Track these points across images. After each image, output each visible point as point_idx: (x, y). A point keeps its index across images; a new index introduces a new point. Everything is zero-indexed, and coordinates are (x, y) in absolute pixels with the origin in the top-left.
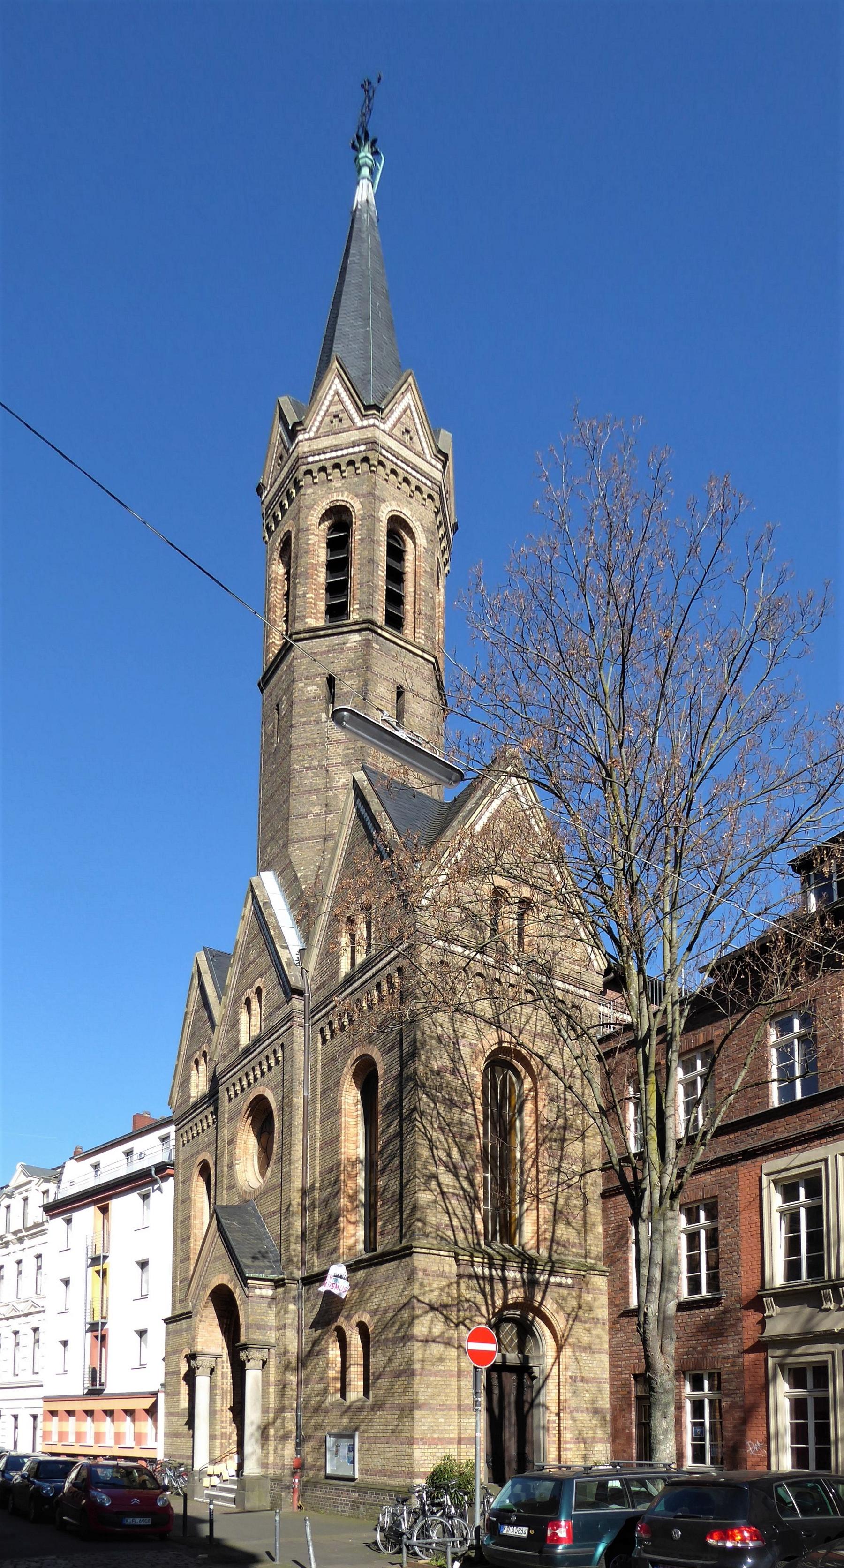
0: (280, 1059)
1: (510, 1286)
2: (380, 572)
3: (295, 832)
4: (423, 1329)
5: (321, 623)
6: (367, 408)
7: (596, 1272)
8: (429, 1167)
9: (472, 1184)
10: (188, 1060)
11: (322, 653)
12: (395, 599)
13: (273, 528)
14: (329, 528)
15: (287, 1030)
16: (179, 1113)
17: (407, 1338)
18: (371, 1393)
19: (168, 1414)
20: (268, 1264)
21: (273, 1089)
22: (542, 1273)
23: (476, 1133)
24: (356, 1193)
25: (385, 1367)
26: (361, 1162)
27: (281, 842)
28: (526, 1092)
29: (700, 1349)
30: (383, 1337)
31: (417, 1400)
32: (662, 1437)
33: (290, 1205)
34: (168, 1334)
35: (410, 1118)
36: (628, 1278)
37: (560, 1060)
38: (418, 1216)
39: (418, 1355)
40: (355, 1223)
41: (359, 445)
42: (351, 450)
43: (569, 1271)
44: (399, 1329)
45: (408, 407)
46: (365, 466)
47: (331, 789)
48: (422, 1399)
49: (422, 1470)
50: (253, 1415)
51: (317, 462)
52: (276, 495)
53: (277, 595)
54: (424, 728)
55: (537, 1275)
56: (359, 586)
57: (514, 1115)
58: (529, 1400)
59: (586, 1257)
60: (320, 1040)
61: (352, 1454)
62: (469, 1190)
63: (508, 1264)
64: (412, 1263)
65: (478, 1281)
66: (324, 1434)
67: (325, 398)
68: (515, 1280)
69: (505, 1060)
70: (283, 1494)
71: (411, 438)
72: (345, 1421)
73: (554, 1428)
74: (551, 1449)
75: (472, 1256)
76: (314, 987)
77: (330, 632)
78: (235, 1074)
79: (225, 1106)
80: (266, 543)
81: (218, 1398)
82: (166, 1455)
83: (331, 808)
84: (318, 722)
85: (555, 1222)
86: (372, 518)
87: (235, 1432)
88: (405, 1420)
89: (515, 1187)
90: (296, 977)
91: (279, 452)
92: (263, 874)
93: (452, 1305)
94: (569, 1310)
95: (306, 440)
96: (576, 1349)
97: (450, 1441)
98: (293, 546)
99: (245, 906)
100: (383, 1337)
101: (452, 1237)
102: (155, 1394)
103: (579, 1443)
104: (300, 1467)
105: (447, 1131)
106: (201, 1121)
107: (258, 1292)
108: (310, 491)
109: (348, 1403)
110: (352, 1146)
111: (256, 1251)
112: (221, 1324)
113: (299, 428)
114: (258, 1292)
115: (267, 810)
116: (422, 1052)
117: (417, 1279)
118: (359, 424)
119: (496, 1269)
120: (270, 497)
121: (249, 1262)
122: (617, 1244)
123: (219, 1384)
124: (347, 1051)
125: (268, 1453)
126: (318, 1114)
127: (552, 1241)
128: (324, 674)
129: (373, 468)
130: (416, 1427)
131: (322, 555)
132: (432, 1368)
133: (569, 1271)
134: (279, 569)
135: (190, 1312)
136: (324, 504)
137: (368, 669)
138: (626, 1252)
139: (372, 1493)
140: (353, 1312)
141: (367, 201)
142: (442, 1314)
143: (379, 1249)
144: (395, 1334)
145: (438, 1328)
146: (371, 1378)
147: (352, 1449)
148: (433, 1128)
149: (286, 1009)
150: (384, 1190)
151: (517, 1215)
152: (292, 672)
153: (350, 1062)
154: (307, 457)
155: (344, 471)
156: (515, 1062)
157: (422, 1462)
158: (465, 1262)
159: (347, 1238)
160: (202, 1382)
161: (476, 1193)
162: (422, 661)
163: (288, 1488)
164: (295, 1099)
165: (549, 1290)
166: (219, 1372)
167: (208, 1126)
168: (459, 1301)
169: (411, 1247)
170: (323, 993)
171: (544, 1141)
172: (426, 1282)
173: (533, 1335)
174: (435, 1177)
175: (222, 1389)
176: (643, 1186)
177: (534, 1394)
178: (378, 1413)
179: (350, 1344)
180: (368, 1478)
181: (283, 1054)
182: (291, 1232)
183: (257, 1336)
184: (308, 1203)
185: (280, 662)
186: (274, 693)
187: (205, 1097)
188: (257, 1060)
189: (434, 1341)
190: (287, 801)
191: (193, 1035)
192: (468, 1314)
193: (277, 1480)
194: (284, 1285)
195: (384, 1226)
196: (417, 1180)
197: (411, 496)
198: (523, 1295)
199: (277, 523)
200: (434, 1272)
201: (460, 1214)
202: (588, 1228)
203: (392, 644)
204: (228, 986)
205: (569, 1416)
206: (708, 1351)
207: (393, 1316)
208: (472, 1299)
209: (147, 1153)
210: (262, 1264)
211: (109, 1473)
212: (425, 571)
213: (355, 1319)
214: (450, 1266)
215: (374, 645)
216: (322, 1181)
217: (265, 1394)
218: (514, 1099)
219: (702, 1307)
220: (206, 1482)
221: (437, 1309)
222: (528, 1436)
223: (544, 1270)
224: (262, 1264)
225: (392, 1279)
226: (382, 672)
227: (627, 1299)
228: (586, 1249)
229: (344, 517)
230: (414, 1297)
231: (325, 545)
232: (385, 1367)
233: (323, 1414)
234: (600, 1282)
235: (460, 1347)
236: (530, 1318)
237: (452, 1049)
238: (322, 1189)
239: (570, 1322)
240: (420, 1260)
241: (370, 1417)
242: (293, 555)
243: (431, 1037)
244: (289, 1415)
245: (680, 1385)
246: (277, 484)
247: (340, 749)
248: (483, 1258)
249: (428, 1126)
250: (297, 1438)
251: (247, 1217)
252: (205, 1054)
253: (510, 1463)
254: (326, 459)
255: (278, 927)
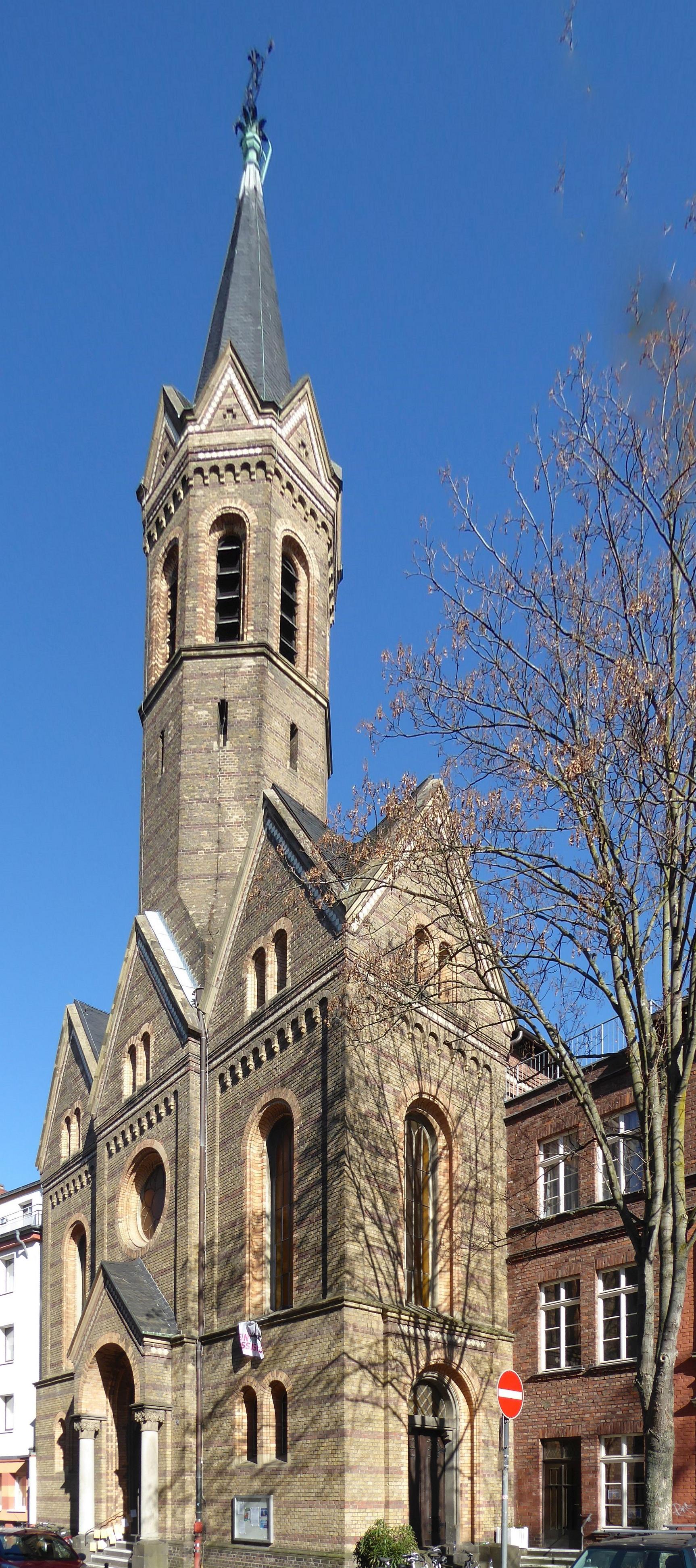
0: (172, 1108)
1: (432, 1346)
2: (275, 595)
3: (185, 866)
4: (353, 1388)
5: (212, 642)
6: (265, 404)
7: (504, 1338)
8: (357, 1217)
9: (396, 1240)
10: (57, 1119)
11: (213, 676)
12: (288, 631)
13: (156, 537)
14: (220, 541)
15: (181, 1076)
16: (48, 1174)
17: (340, 1397)
18: (289, 1455)
19: (41, 1478)
20: (163, 1322)
21: (163, 1141)
22: (460, 1336)
23: (399, 1186)
24: (262, 1248)
25: (307, 1428)
26: (267, 1216)
27: (168, 880)
28: (440, 1150)
29: (619, 1413)
30: (304, 1397)
31: (348, 1462)
32: (661, 1499)
33: (187, 1260)
34: (39, 1398)
35: (337, 1162)
36: (536, 1343)
37: (472, 1119)
38: (346, 1268)
39: (348, 1416)
40: (261, 1280)
41: (254, 447)
42: (245, 452)
43: (483, 1335)
44: (325, 1388)
45: (304, 418)
46: (260, 473)
47: (223, 825)
48: (352, 1461)
49: (353, 1535)
50: (149, 1479)
51: (208, 460)
52: (160, 498)
53: (160, 612)
54: (316, 775)
55: (456, 1337)
56: (253, 606)
57: (427, 1173)
58: (442, 1464)
59: (493, 1322)
60: (218, 1087)
61: (265, 1518)
62: (392, 1245)
63: (432, 1323)
64: (342, 1318)
65: (404, 1339)
66: (230, 1498)
67: (218, 387)
68: (437, 1342)
69: (421, 1114)
70: (185, 1559)
71: (307, 454)
72: (257, 1484)
73: (467, 1492)
74: (464, 1513)
75: (400, 1313)
76: (212, 1030)
77: (222, 652)
78: (117, 1127)
79: (105, 1163)
80: (147, 554)
81: (103, 1461)
82: (38, 1519)
83: (223, 846)
84: (209, 750)
85: (467, 1285)
86: (267, 531)
87: (122, 1496)
88: (333, 1483)
89: (428, 1248)
90: (193, 1018)
91: (164, 449)
92: (149, 914)
93: (379, 1364)
94: (482, 1374)
95: (197, 433)
96: (488, 1414)
97: (377, 1505)
98: (180, 554)
99: (129, 947)
100: (304, 1397)
101: (377, 1294)
102: (26, 1459)
103: (490, 1506)
104: (201, 1531)
105: (372, 1180)
106: (74, 1181)
107: (154, 1350)
108: (200, 492)
109: (259, 1465)
110: (257, 1199)
111: (150, 1309)
112: (105, 1386)
113: (189, 418)
114: (154, 1350)
115: (151, 847)
116: (351, 1092)
117: (347, 1335)
118: (255, 422)
119: (420, 1328)
120: (152, 501)
121: (144, 1319)
122: (524, 1310)
123: (104, 1447)
124: (252, 1097)
125: (166, 1517)
126: (217, 1166)
127: (465, 1304)
128: (216, 698)
129: (269, 476)
130: (347, 1491)
131: (211, 569)
132: (361, 1429)
133: (483, 1335)
134: (162, 585)
135: (72, 1374)
136: (216, 509)
137: (263, 698)
138: (535, 1318)
139: (293, 1559)
140: (266, 1371)
141: (255, 188)
142: (370, 1372)
143: (296, 1305)
144: (320, 1393)
145: (367, 1388)
146: (289, 1439)
147: (266, 1513)
148: (361, 1175)
149: (181, 1053)
150: (301, 1243)
151: (430, 1277)
152: (181, 693)
153: (256, 1109)
154: (197, 453)
155: (238, 475)
156: (430, 1117)
157: (352, 1527)
158: (392, 1319)
159: (254, 1295)
160: (86, 1446)
161: (399, 1248)
162: (315, 703)
163: (193, 1552)
164: (191, 1150)
165: (465, 1352)
166: (103, 1435)
167: (82, 1186)
168: (387, 1359)
169: (342, 1300)
170: (225, 1035)
171: (458, 1202)
172: (355, 1338)
173: (447, 1398)
174: (361, 1227)
175: (107, 1452)
176: (652, 1223)
177: (446, 1458)
178: (299, 1476)
179: (262, 1404)
180: (286, 1543)
181: (177, 1103)
182: (189, 1289)
183: (152, 1397)
184: (205, 1259)
185: (166, 684)
186: (159, 719)
187: (79, 1155)
188: (144, 1111)
189: (363, 1401)
190: (176, 834)
191: (63, 1092)
192: (395, 1374)
193: (177, 1545)
194: (182, 1344)
195: (302, 1280)
196: (346, 1229)
197: (305, 520)
198: (443, 1357)
199: (160, 530)
200: (364, 1328)
201: (384, 1269)
202: (495, 1294)
203: (286, 677)
204: (109, 1035)
205: (482, 1479)
206: (629, 1415)
207: (317, 1375)
208: (399, 1359)
209: (9, 1218)
210: (156, 1322)
211: (14, 1540)
212: (318, 606)
213: (269, 1378)
214: (378, 1322)
215: (269, 673)
216: (222, 1236)
217: (162, 1456)
218: (428, 1157)
219: (623, 1372)
220: (93, 1546)
221: (366, 1368)
222: (441, 1500)
223: (462, 1332)
224: (156, 1322)
225: (316, 1335)
226: (277, 705)
227: (535, 1364)
228: (493, 1315)
229: (236, 529)
230: (344, 1353)
231: (215, 558)
232: (307, 1428)
233: (228, 1477)
234: (506, 1347)
235: (387, 1407)
236: (446, 1381)
237: (377, 1093)
238: (222, 1244)
239: (484, 1386)
240: (350, 1315)
241: (288, 1480)
242: (180, 563)
243: (359, 1077)
244: (189, 1478)
245: (596, 1449)
246: (161, 485)
247: (233, 783)
248: (410, 1316)
249: (356, 1172)
250: (197, 1501)
251: (136, 1275)
252: (77, 1112)
253: (425, 1526)
254: (218, 458)
255: (169, 967)
